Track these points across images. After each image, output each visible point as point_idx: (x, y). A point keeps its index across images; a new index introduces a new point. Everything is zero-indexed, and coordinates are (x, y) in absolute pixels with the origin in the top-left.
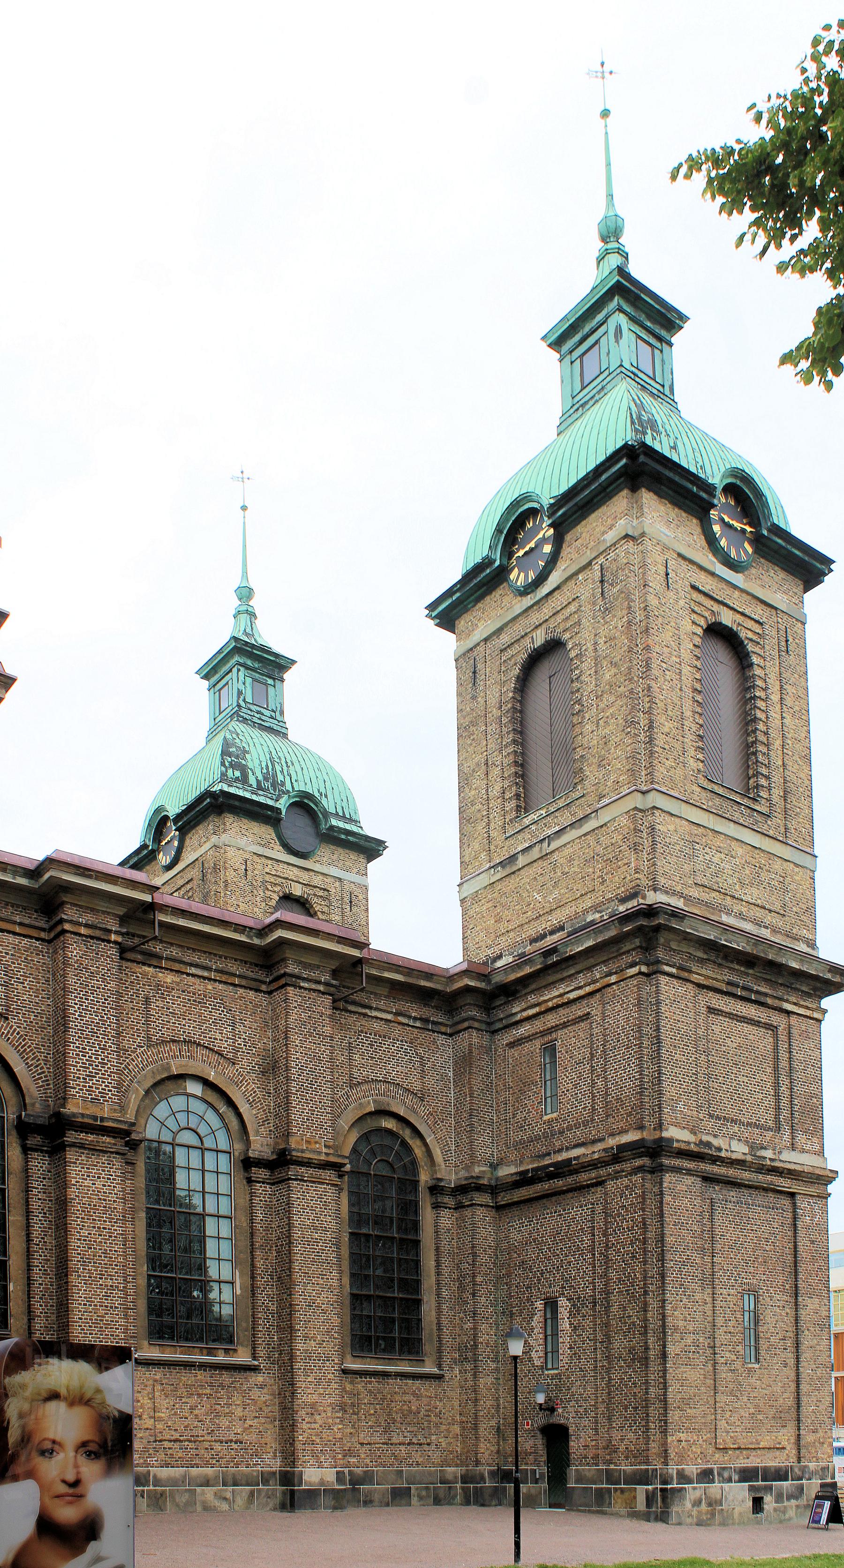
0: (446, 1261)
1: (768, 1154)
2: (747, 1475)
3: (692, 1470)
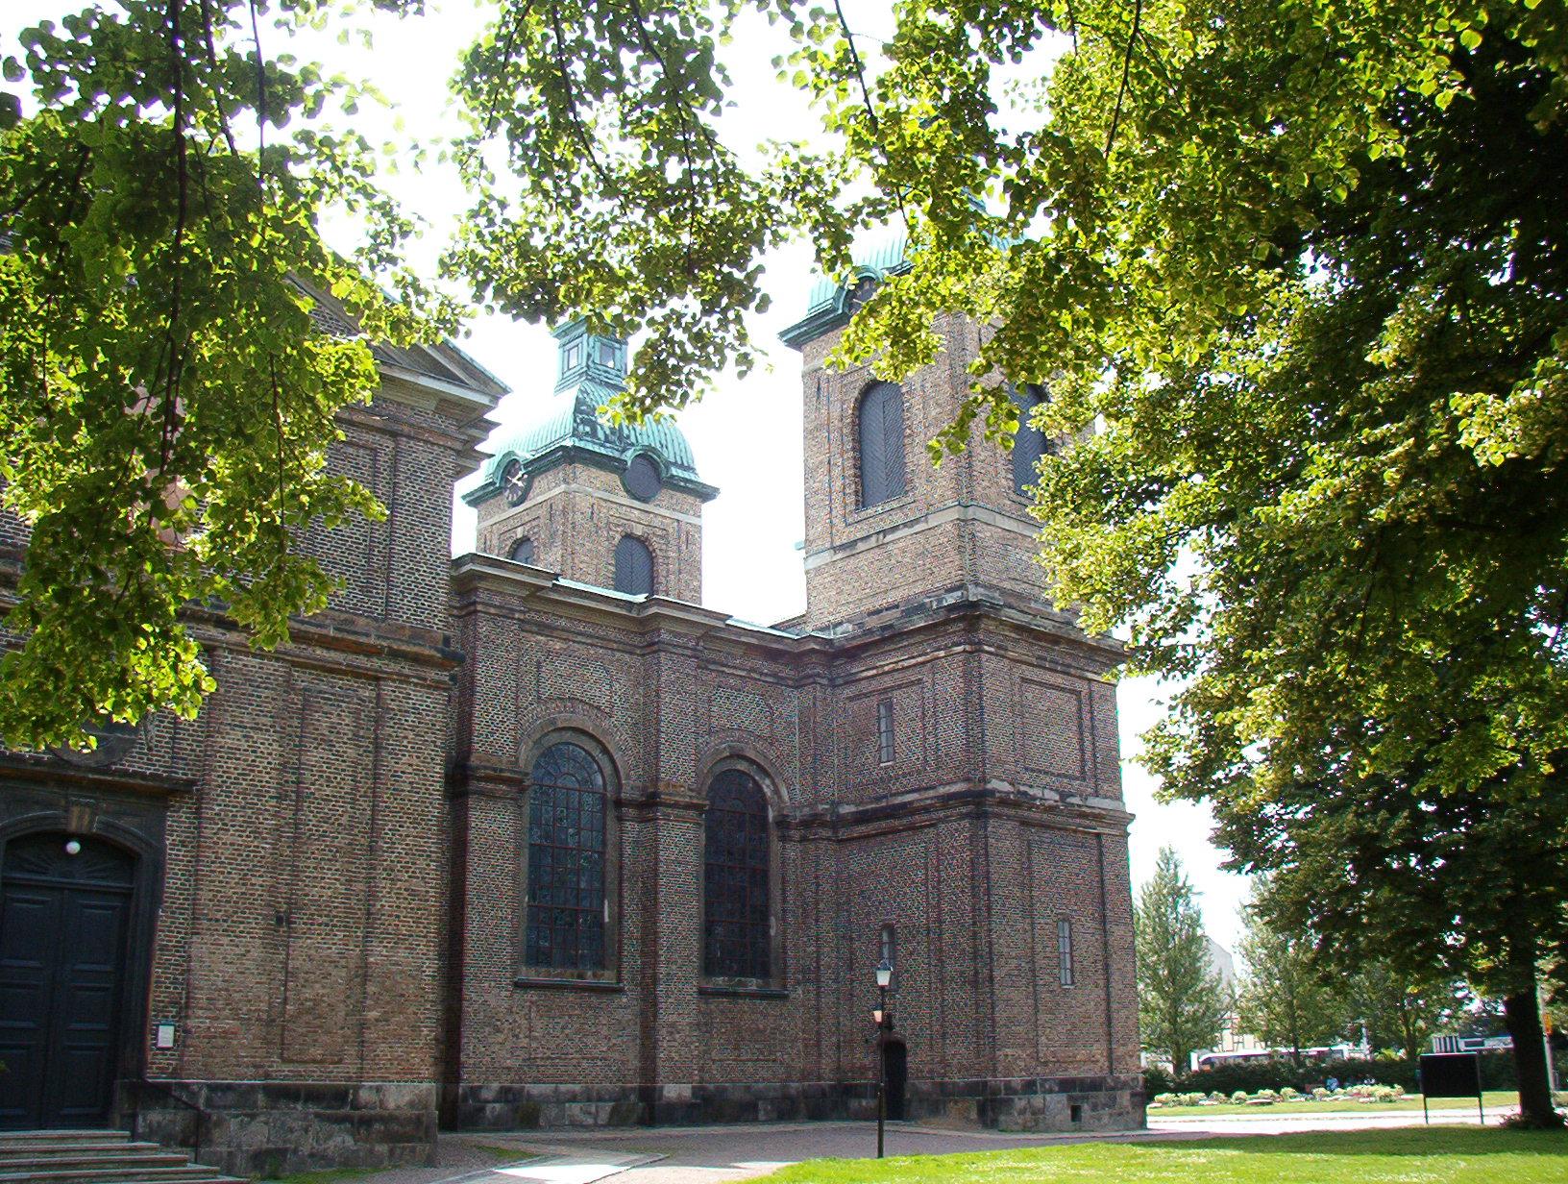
0: (791, 888)
1: (1076, 800)
2: (1066, 1085)
3: (1016, 1081)
